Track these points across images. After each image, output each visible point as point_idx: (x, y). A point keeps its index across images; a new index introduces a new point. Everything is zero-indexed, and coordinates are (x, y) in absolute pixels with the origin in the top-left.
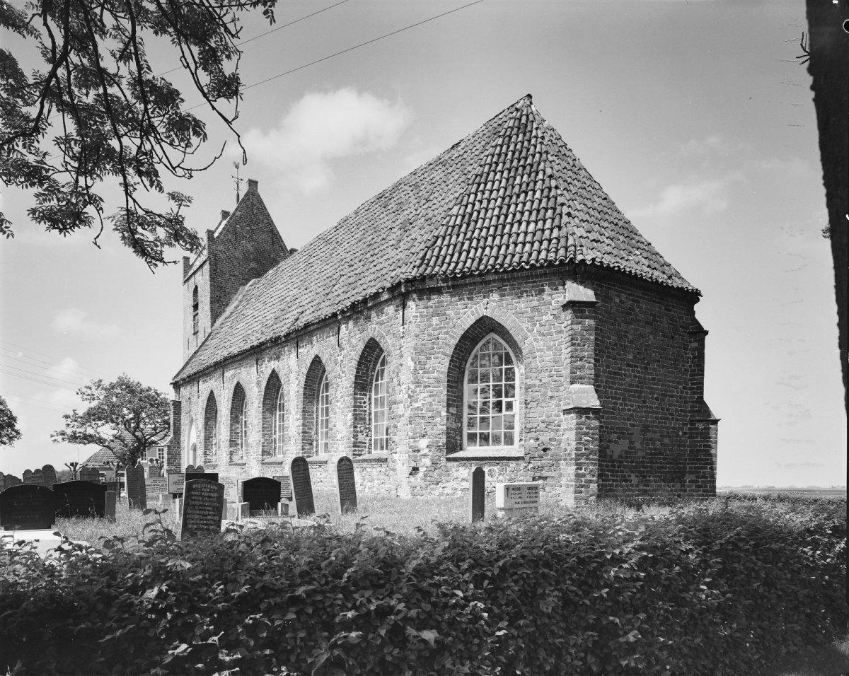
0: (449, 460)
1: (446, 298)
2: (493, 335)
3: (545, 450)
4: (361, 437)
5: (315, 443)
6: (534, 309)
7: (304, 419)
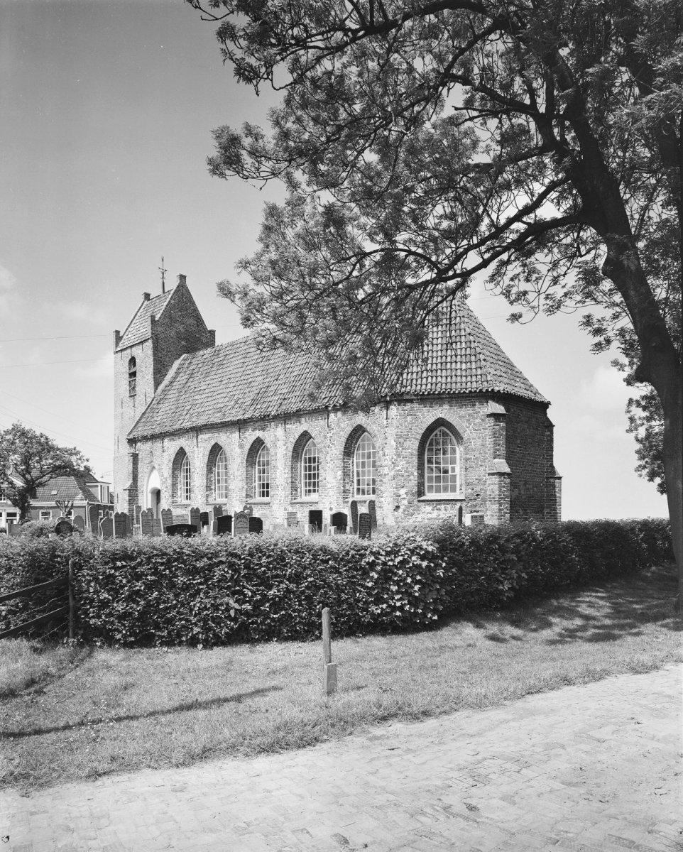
0: (419, 501)
1: (416, 405)
2: (443, 428)
3: (477, 495)
4: (348, 487)
5: (299, 490)
6: (469, 415)
7: (292, 473)
